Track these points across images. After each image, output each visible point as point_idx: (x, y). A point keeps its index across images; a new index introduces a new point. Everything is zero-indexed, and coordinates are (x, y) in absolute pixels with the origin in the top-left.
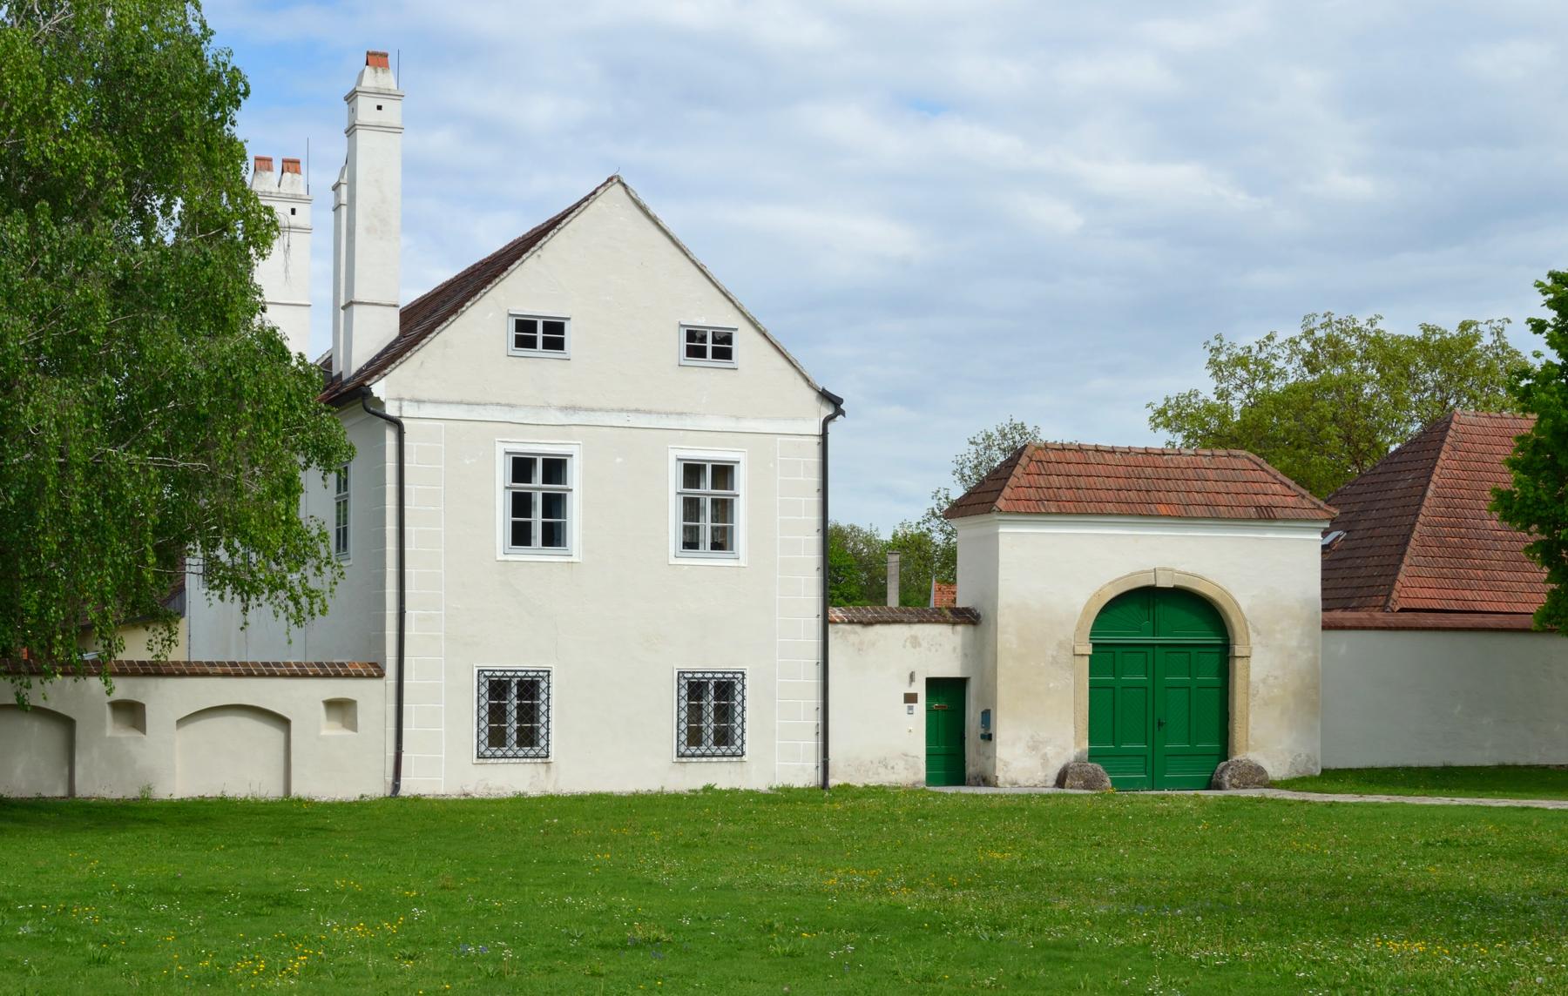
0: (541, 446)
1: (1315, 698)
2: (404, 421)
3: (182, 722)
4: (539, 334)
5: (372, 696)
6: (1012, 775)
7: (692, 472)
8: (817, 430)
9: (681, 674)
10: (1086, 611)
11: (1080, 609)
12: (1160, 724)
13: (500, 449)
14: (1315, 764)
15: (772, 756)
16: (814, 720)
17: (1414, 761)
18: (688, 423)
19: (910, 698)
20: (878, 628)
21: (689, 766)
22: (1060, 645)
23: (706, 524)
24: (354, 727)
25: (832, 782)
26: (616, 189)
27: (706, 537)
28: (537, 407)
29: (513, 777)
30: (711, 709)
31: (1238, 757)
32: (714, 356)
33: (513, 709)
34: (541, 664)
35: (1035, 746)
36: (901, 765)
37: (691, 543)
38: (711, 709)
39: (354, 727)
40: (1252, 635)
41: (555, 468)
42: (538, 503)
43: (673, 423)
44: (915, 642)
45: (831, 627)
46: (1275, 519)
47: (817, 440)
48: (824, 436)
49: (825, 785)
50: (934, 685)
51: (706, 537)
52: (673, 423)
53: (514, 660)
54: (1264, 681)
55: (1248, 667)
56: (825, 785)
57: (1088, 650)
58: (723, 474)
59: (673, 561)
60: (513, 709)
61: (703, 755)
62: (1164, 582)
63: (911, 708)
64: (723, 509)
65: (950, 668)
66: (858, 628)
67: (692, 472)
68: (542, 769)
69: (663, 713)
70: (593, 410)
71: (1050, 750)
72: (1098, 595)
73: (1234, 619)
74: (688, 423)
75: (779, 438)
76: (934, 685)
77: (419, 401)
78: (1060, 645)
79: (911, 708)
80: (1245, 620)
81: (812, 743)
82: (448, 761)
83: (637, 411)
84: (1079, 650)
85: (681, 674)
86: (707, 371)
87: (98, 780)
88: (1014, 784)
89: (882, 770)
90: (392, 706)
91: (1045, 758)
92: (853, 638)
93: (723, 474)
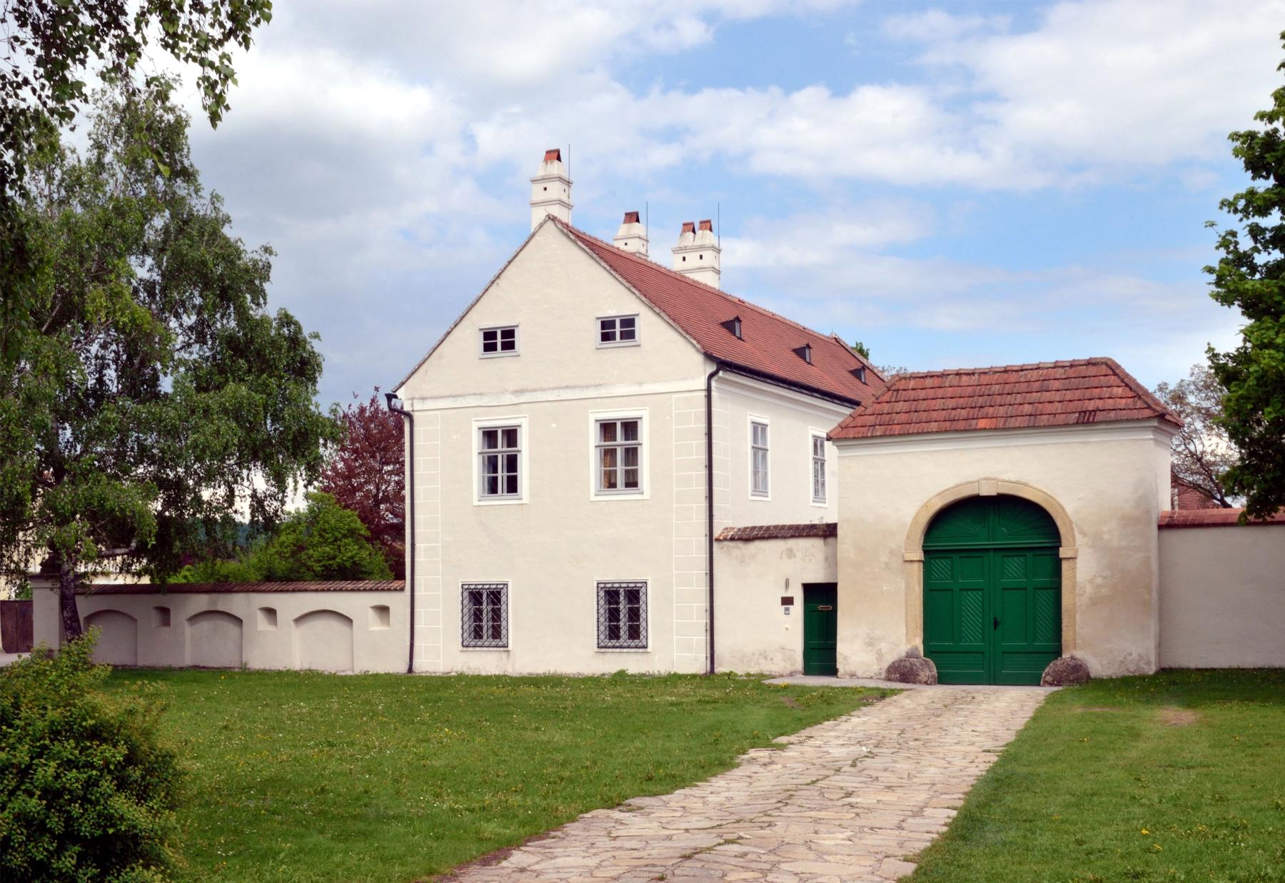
0: (499, 421)
1: (1160, 600)
2: (416, 416)
3: (299, 620)
4: (499, 340)
5: (397, 601)
6: (851, 668)
7: (607, 429)
8: (703, 386)
9: (506, 585)
10: (915, 521)
11: (909, 520)
12: (996, 623)
13: (475, 426)
14: (1149, 663)
15: (671, 648)
16: (704, 620)
17: (1250, 660)
18: (603, 392)
19: (787, 601)
20: (757, 544)
21: (608, 656)
22: (892, 553)
23: (502, 475)
24: (388, 624)
25: (718, 670)
26: (550, 224)
27: (620, 479)
28: (496, 391)
29: (485, 662)
30: (622, 611)
31: (1066, 655)
32: (503, 348)
33: (485, 611)
34: (504, 580)
35: (871, 643)
36: (779, 657)
37: (493, 488)
38: (622, 611)
39: (388, 624)
40: (1078, 537)
41: (511, 435)
42: (501, 464)
43: (591, 393)
44: (791, 554)
45: (715, 545)
46: (1094, 423)
47: (704, 394)
48: (709, 390)
49: (410, 670)
50: (809, 589)
51: (620, 479)
52: (591, 393)
53: (484, 577)
54: (1091, 581)
55: (1074, 569)
56: (410, 670)
57: (919, 555)
58: (631, 428)
59: (593, 498)
60: (485, 611)
61: (621, 647)
62: (987, 490)
63: (787, 609)
64: (632, 455)
65: (817, 577)
66: (740, 544)
67: (607, 429)
68: (505, 655)
69: (588, 613)
70: (535, 390)
71: (884, 646)
72: (926, 505)
73: (1059, 523)
74: (603, 392)
75: (674, 396)
76: (809, 589)
77: (423, 399)
78: (892, 553)
79: (787, 609)
80: (1071, 522)
81: (703, 638)
82: (443, 650)
83: (567, 387)
84: (908, 557)
85: (506, 585)
86: (618, 352)
87: (258, 660)
88: (853, 675)
89: (762, 661)
90: (409, 610)
91: (880, 655)
92: (736, 552)
93: (631, 428)
